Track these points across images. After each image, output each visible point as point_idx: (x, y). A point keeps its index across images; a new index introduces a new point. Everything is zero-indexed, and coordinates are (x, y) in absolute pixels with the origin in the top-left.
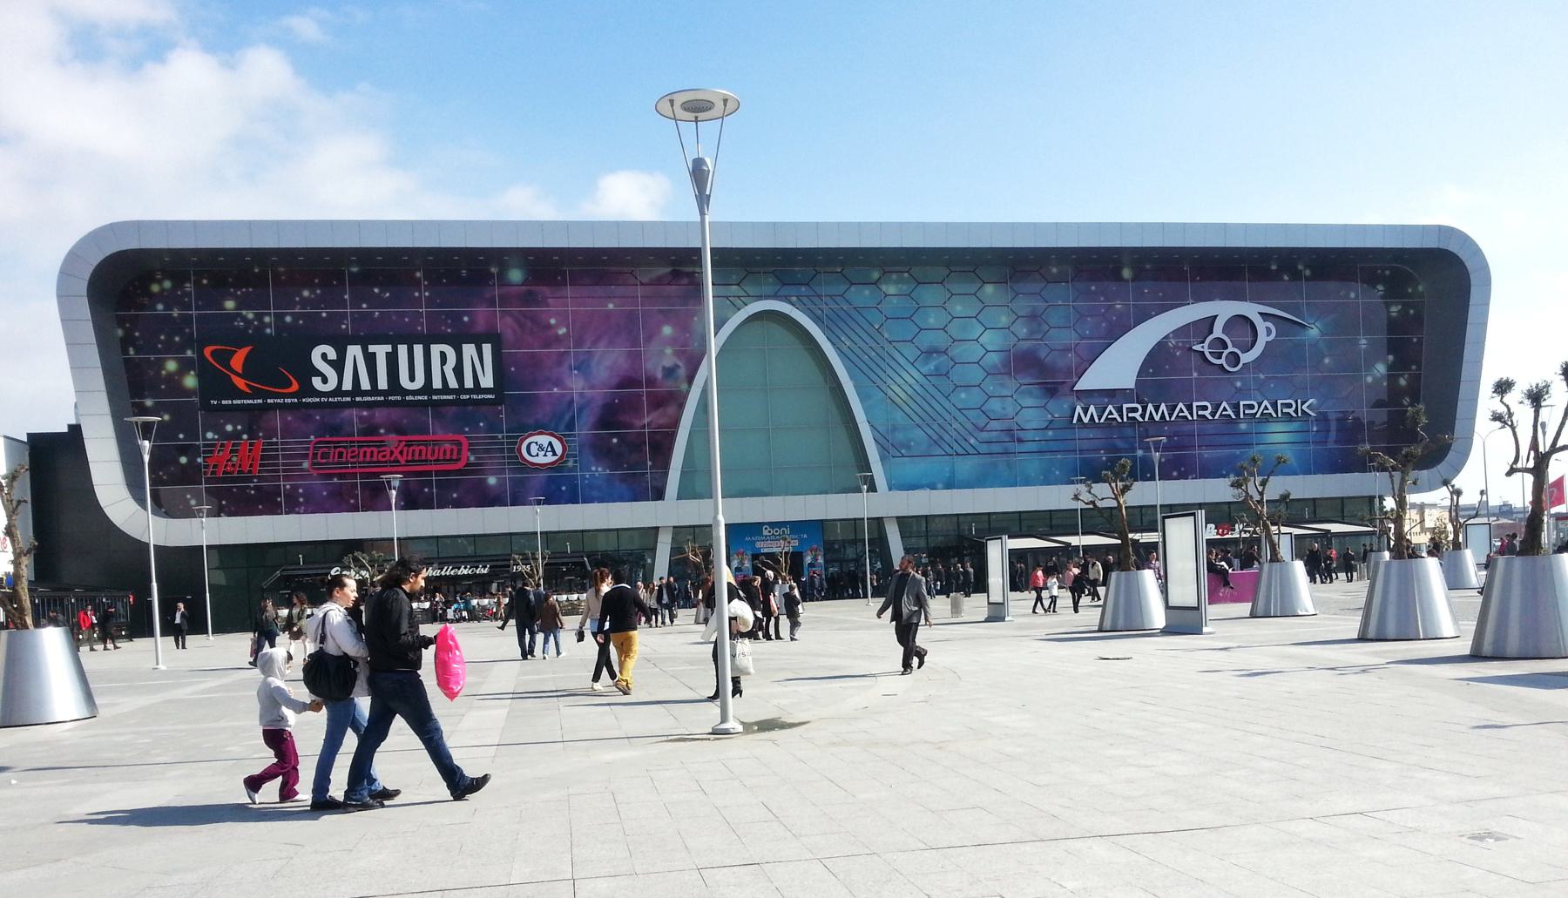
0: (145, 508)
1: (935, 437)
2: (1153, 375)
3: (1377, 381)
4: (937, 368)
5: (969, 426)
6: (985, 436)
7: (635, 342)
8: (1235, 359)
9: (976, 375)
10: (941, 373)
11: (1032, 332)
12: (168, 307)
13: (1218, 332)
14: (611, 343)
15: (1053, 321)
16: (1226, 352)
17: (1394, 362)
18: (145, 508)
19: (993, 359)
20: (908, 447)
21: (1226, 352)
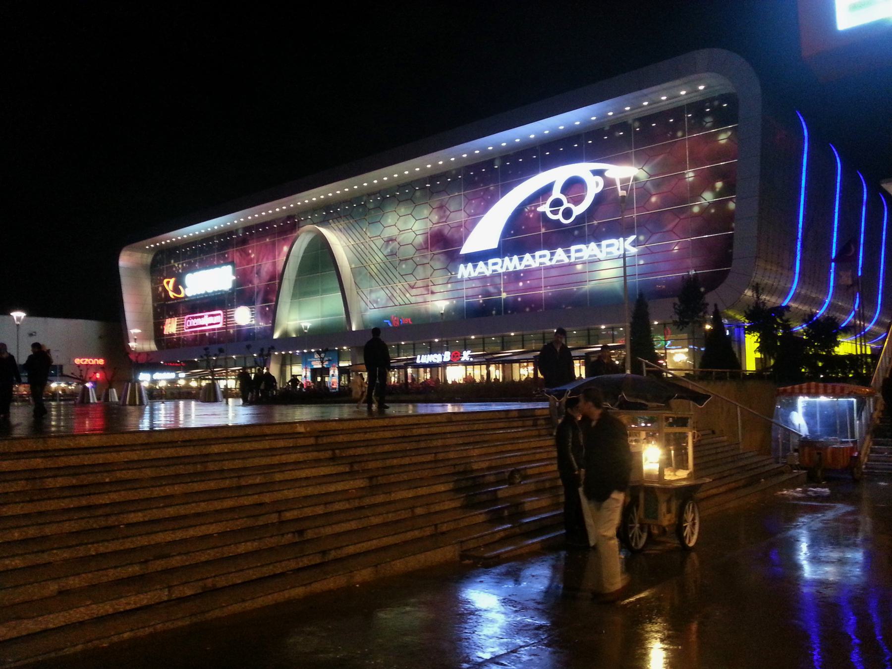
0: (728, 272)
1: (390, 295)
2: (514, 235)
3: (704, 210)
4: (391, 251)
5: (407, 286)
6: (414, 292)
7: (275, 258)
8: (567, 213)
9: (411, 251)
10: (393, 254)
11: (441, 218)
12: (294, 354)
13: (556, 194)
14: (267, 259)
15: (452, 209)
16: (562, 209)
17: (722, 189)
18: (728, 272)
19: (420, 239)
20: (377, 302)
21: (562, 209)
